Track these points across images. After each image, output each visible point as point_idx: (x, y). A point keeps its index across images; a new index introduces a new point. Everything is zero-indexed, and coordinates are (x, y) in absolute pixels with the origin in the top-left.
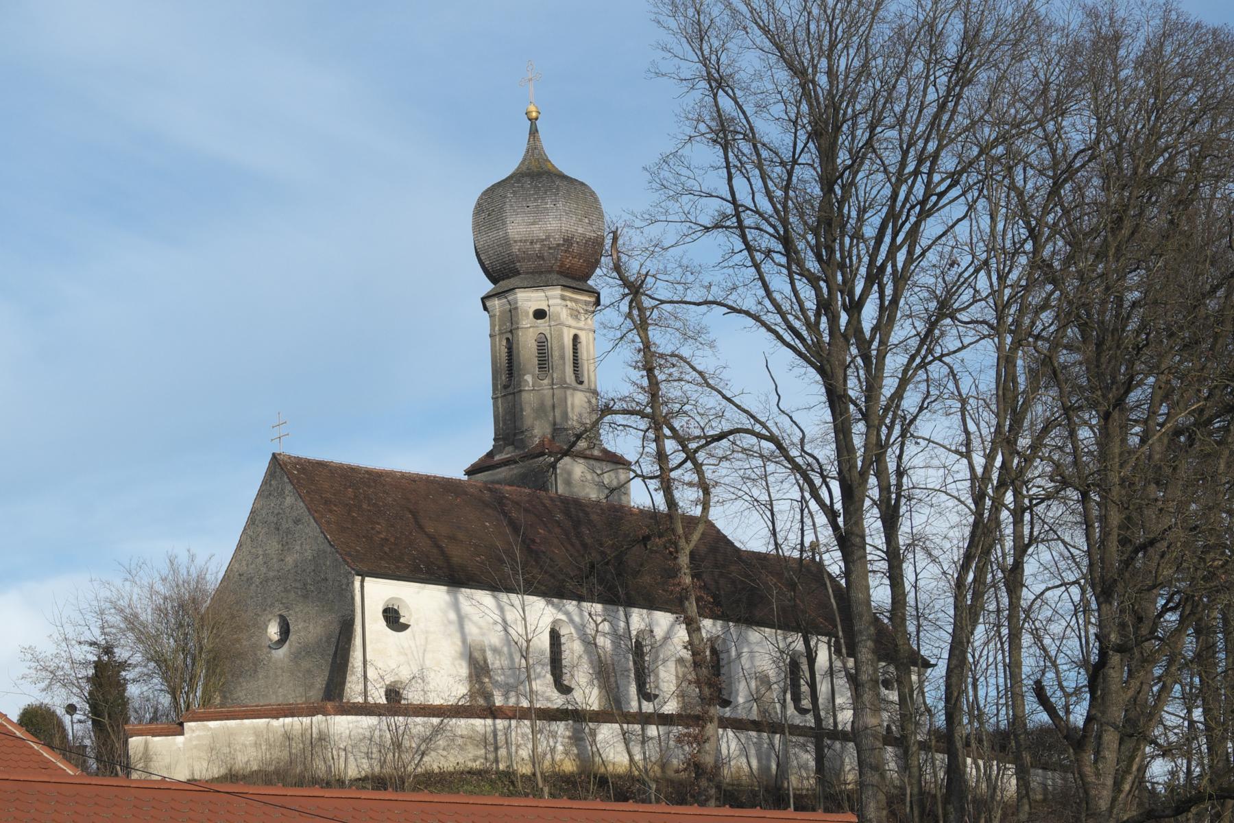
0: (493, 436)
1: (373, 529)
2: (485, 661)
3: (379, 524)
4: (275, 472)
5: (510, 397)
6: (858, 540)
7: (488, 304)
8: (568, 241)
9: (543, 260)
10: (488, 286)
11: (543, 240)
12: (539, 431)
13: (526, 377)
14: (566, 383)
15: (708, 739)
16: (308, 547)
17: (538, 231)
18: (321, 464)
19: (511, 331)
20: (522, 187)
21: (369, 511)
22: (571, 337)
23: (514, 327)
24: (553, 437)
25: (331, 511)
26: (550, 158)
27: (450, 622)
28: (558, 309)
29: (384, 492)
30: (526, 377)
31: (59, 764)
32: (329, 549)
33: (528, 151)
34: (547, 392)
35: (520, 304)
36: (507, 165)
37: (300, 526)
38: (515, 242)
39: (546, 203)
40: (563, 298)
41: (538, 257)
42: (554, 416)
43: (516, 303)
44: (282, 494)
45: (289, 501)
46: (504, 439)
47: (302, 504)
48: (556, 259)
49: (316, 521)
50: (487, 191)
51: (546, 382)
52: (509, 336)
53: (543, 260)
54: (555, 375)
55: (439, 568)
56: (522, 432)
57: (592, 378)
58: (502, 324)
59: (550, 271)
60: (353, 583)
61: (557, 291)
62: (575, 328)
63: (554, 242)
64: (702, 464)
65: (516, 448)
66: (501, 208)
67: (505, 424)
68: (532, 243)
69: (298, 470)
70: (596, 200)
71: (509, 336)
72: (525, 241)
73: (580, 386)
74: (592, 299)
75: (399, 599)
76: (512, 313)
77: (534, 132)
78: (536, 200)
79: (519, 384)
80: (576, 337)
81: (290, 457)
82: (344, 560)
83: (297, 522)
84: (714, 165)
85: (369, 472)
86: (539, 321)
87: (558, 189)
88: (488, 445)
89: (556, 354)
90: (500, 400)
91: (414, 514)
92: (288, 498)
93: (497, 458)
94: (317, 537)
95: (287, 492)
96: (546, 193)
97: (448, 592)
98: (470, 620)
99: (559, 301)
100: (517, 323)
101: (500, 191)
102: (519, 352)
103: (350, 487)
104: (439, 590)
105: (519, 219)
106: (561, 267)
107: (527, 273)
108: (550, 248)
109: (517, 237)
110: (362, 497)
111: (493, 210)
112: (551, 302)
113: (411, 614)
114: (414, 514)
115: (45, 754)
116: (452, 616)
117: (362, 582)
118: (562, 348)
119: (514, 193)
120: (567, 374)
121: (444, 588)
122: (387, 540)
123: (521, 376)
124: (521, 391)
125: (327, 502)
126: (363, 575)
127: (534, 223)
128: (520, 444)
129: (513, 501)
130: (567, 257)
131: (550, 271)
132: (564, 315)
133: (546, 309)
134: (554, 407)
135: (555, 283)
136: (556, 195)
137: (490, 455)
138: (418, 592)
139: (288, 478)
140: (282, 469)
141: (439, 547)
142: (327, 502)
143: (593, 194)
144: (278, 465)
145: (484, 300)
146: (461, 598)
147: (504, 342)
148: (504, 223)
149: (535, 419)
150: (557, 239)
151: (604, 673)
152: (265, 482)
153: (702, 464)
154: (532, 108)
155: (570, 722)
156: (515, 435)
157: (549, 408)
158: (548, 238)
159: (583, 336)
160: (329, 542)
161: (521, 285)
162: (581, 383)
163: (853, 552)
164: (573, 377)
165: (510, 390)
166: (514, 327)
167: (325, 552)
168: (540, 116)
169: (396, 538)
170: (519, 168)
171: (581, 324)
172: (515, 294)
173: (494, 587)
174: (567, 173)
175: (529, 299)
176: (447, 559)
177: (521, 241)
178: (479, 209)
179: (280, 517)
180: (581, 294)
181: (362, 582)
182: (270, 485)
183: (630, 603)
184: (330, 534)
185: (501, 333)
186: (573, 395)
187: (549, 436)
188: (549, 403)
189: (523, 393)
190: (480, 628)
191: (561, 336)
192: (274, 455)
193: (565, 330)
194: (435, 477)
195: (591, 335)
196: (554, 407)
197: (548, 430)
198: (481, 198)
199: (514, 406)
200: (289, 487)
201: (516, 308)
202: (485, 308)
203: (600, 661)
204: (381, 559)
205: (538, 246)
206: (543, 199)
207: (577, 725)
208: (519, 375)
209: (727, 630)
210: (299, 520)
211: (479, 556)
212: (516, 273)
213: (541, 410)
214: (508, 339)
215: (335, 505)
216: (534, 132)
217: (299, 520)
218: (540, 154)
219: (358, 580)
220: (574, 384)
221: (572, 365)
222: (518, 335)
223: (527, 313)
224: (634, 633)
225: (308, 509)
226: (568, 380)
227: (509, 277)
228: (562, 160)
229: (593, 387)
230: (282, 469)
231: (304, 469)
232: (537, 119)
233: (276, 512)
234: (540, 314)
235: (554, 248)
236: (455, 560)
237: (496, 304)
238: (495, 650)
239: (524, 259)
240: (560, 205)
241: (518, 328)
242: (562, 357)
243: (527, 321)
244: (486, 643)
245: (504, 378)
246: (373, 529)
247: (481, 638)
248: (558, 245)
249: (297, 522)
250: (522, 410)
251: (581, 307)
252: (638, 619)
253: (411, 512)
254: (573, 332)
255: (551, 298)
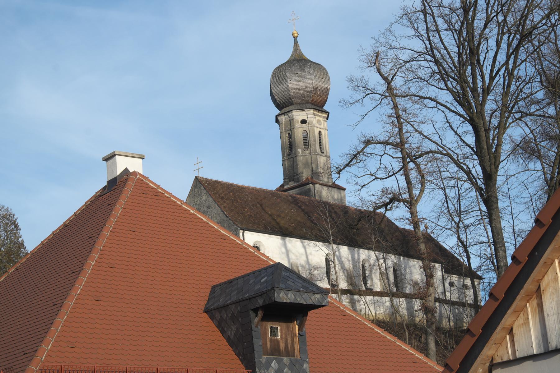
0: (283, 178)
1: (244, 210)
2: (299, 271)
3: (246, 208)
4: (197, 185)
5: (291, 159)
6: (495, 199)
7: (279, 118)
8: (315, 89)
9: (304, 97)
10: (278, 112)
11: (304, 89)
12: (305, 174)
13: (298, 150)
14: (317, 152)
15: (431, 294)
16: (215, 219)
17: (302, 85)
18: (217, 182)
19: (291, 130)
20: (294, 65)
21: (241, 203)
22: (318, 132)
23: (292, 127)
24: (312, 176)
25: (225, 202)
26: (304, 54)
27: (283, 253)
28: (312, 119)
29: (246, 195)
30: (298, 150)
31: (231, 237)
32: (226, 219)
33: (294, 51)
34: (308, 156)
35: (294, 117)
36: (285, 56)
37: (211, 209)
38: (292, 89)
39: (305, 72)
40: (314, 114)
41: (302, 96)
42: (312, 167)
43: (293, 117)
44: (200, 195)
45: (204, 198)
46: (288, 178)
47: (211, 199)
48: (310, 97)
49: (219, 206)
50: (277, 67)
51: (308, 152)
52: (290, 132)
53: (304, 97)
54: (312, 149)
55: (276, 228)
56: (298, 175)
57: (328, 151)
58: (286, 126)
59: (307, 103)
60: (239, 234)
61: (311, 111)
62: (319, 128)
63: (309, 89)
64: (419, 165)
65: (295, 182)
66: (285, 74)
67: (289, 172)
68: (299, 90)
69: (207, 184)
70: (326, 71)
71: (290, 132)
72: (296, 89)
73: (322, 154)
74: (326, 116)
75: (259, 242)
76: (291, 121)
77: (296, 43)
78: (300, 71)
79: (295, 153)
80: (320, 132)
81: (203, 178)
82: (234, 223)
83: (209, 207)
84: (405, 35)
85: (238, 187)
86: (303, 125)
87: (310, 66)
88: (281, 182)
89: (312, 139)
90: (286, 161)
91: (261, 205)
92: (204, 197)
93: (286, 187)
94: (219, 214)
95: (203, 194)
96: (305, 68)
97: (281, 239)
98: (292, 252)
99: (312, 116)
100: (294, 126)
101: (284, 67)
102: (295, 139)
103: (231, 192)
104: (277, 238)
105: (293, 79)
106: (312, 101)
107: (297, 104)
108: (307, 92)
109: (293, 87)
110: (237, 197)
111: (281, 76)
112: (309, 116)
113: (265, 249)
114: (261, 205)
115: (222, 232)
116: (284, 250)
117: (243, 233)
118: (314, 136)
119: (290, 67)
120: (317, 148)
121: (280, 237)
122: (251, 215)
123: (296, 150)
124: (296, 156)
125: (222, 198)
126: (244, 230)
127: (300, 81)
128: (298, 180)
129: (301, 202)
130: (315, 96)
131: (307, 103)
132: (315, 122)
133: (307, 119)
134: (312, 163)
135: (310, 107)
136: (309, 68)
137: (282, 186)
138: (268, 239)
139: (204, 187)
140: (200, 183)
141: (274, 219)
142: (222, 198)
143: (325, 69)
144: (198, 181)
145: (277, 117)
146: (287, 242)
147: (287, 135)
148: (286, 81)
149: (304, 168)
150: (311, 88)
151: (350, 278)
152: (192, 190)
153: (419, 165)
154: (295, 32)
155: (349, 295)
156: (294, 176)
157: (310, 164)
158: (306, 87)
159: (322, 131)
160: (226, 215)
161: (295, 109)
162: (323, 153)
163: (492, 205)
164: (320, 150)
165: (291, 156)
166: (292, 127)
167: (224, 220)
168: (298, 36)
169: (255, 215)
170: (290, 58)
171: (322, 126)
172: (292, 113)
173: (302, 237)
174: (311, 61)
175: (298, 115)
176: (279, 224)
177: (294, 89)
178: (274, 75)
179: (200, 206)
180: (322, 113)
181: (243, 233)
182: (195, 191)
183: (360, 246)
184: (226, 212)
185: (286, 131)
186: (320, 158)
187: (310, 176)
188: (310, 161)
189: (297, 157)
190: (296, 256)
191: (314, 132)
192: (196, 177)
193: (315, 128)
194: (267, 190)
195: (326, 131)
196: (312, 163)
197: (310, 173)
198: (274, 71)
199: (293, 163)
200: (204, 191)
201: (293, 119)
202: (277, 121)
203: (348, 273)
204: (250, 223)
205: (302, 91)
206: (304, 70)
207: (352, 296)
208: (295, 149)
209: (399, 259)
210: (210, 206)
211: (292, 224)
212: (292, 104)
213: (306, 164)
214: (289, 134)
215: (226, 200)
216: (296, 43)
217: (210, 206)
218: (299, 52)
219: (241, 232)
220: (320, 153)
221: (319, 145)
222: (294, 131)
223: (298, 121)
224: (361, 260)
225: (214, 201)
226: (318, 151)
227: (288, 106)
228: (308, 54)
229: (328, 155)
230: (200, 183)
231: (210, 184)
232: (297, 37)
233: (197, 204)
234: (304, 122)
235: (309, 92)
236: (282, 225)
237: (283, 118)
238: (303, 267)
239: (295, 97)
240: (311, 73)
241: (294, 128)
242: (315, 141)
243: (298, 125)
244: (299, 263)
245: (287, 151)
246: (244, 210)
247: (296, 261)
248: (311, 91)
249: (209, 207)
250: (297, 165)
251: (321, 119)
252: (364, 254)
253: (259, 204)
254: (319, 130)
255: (309, 114)
